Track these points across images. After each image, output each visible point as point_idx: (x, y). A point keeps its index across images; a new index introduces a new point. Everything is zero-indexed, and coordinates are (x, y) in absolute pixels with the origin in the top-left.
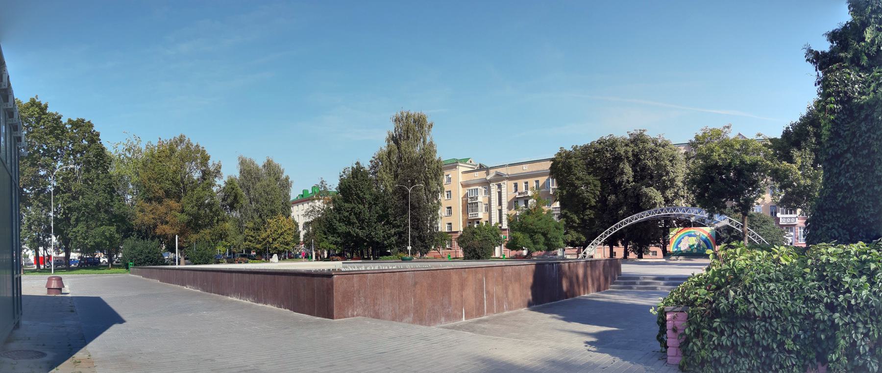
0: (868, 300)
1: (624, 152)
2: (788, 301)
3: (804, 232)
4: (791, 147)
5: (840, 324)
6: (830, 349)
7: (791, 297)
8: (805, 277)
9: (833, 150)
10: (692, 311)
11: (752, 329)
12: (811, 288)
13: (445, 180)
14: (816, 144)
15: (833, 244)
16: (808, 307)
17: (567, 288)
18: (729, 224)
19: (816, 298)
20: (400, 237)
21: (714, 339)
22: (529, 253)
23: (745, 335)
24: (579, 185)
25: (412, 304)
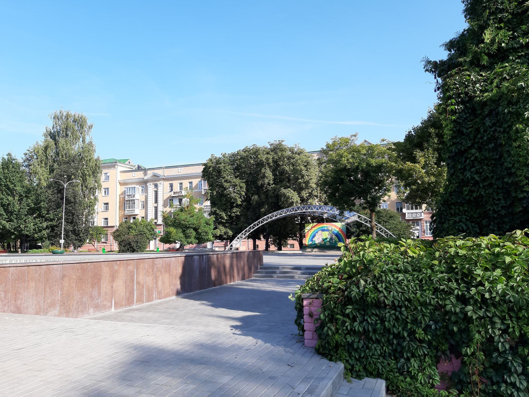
0: (504, 294)
1: (266, 159)
2: (417, 292)
3: (430, 226)
4: (414, 148)
5: (474, 318)
6: (464, 343)
7: (419, 288)
8: (434, 269)
9: (456, 148)
10: (326, 298)
11: (382, 317)
12: (440, 279)
13: (103, 178)
14: (438, 144)
15: (462, 237)
16: (438, 298)
17: (215, 276)
18: (358, 220)
19: (446, 289)
20: (53, 230)
21: (347, 324)
22: (182, 246)
23: (376, 322)
24: (227, 187)
25: (58, 297)
